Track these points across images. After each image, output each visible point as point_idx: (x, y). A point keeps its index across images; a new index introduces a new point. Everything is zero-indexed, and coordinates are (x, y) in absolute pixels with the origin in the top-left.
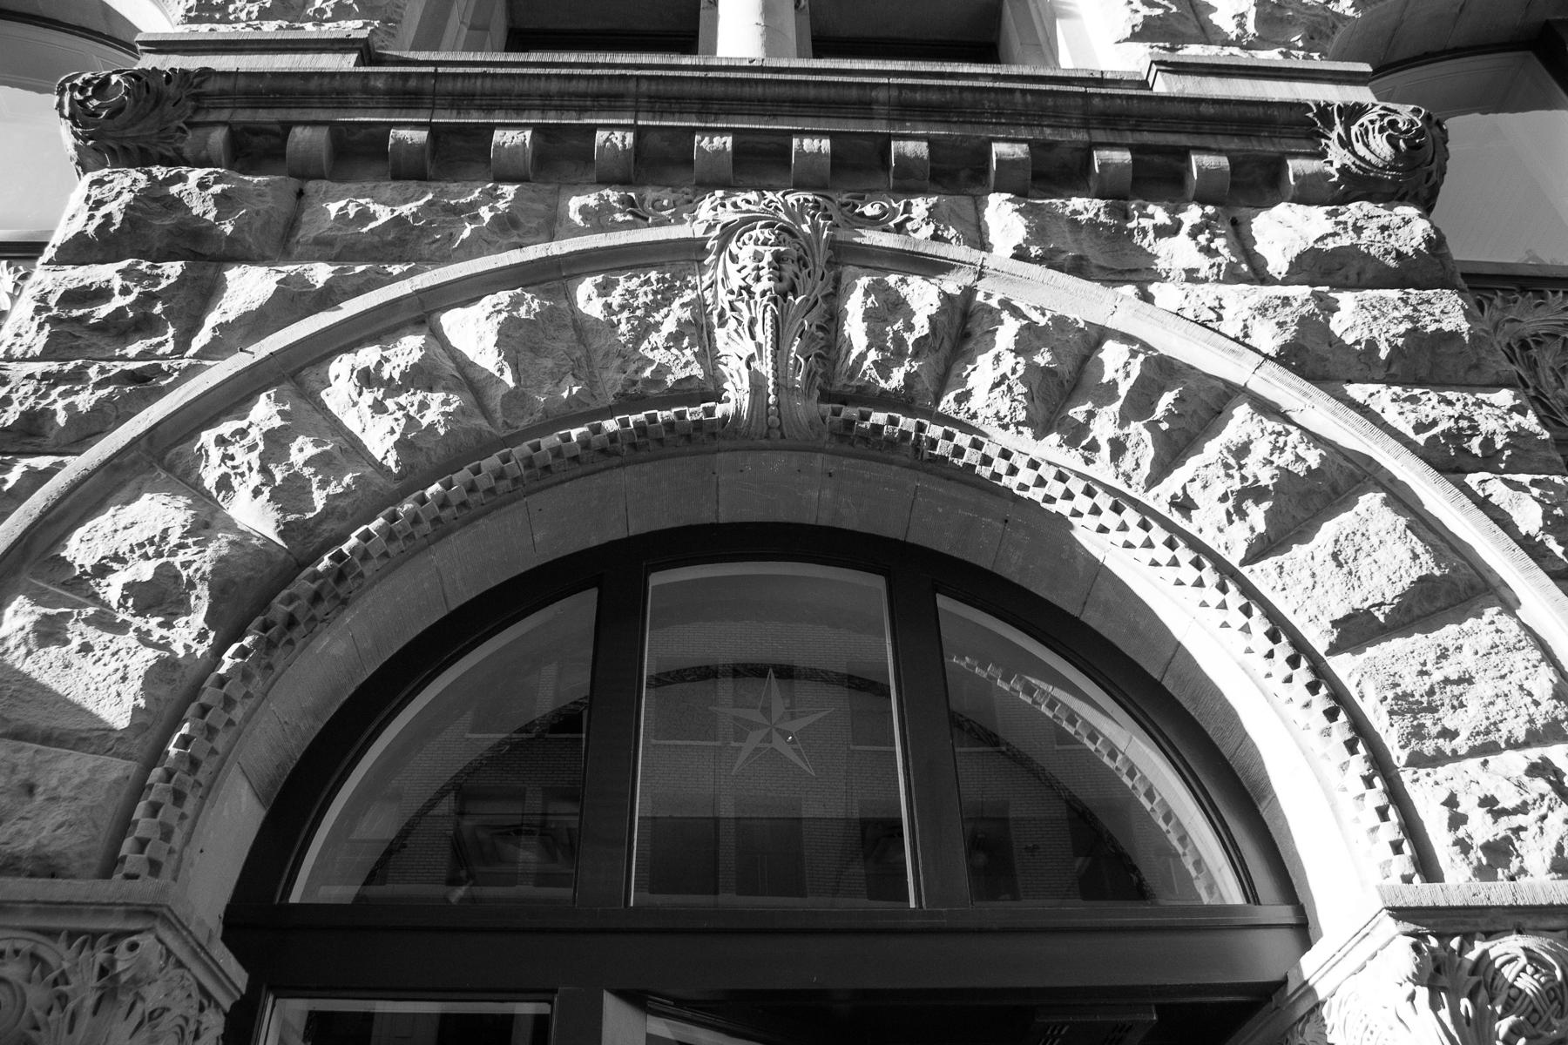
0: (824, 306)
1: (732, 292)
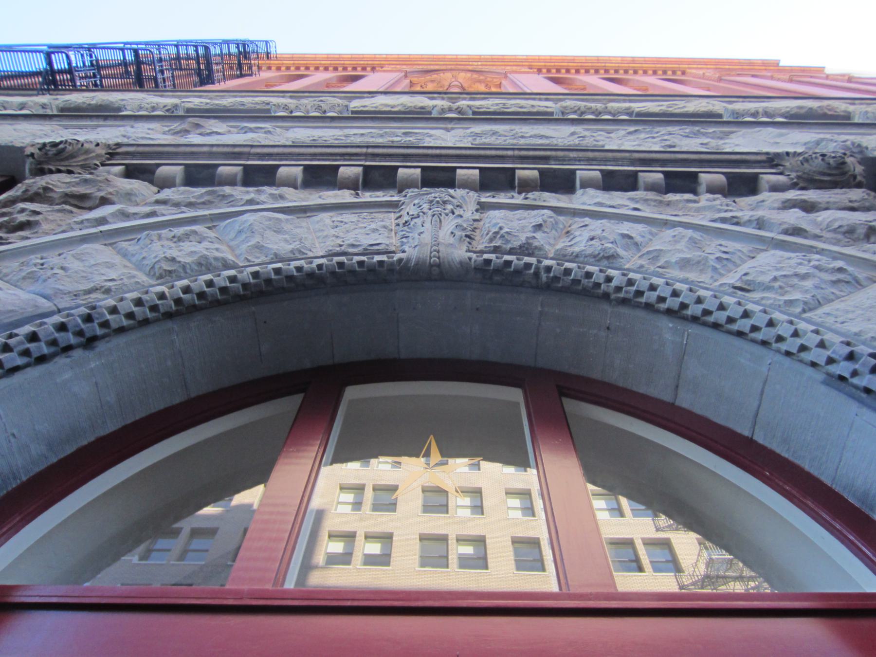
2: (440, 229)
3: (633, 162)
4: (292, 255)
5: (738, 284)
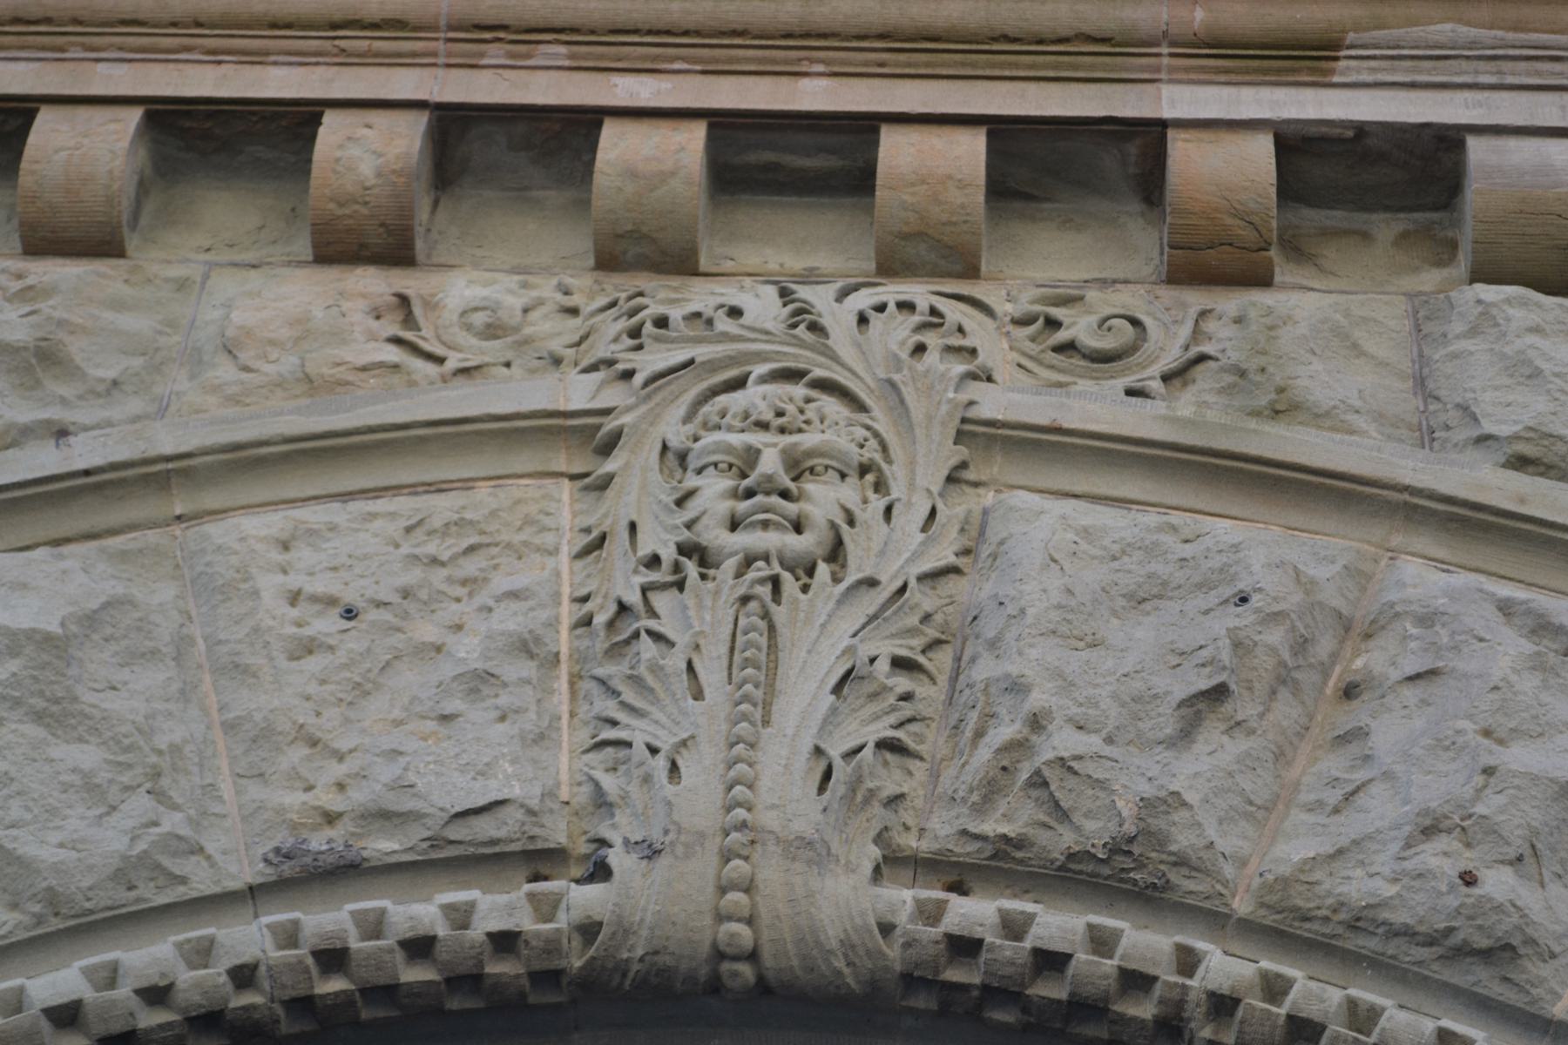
2: (766, 722)
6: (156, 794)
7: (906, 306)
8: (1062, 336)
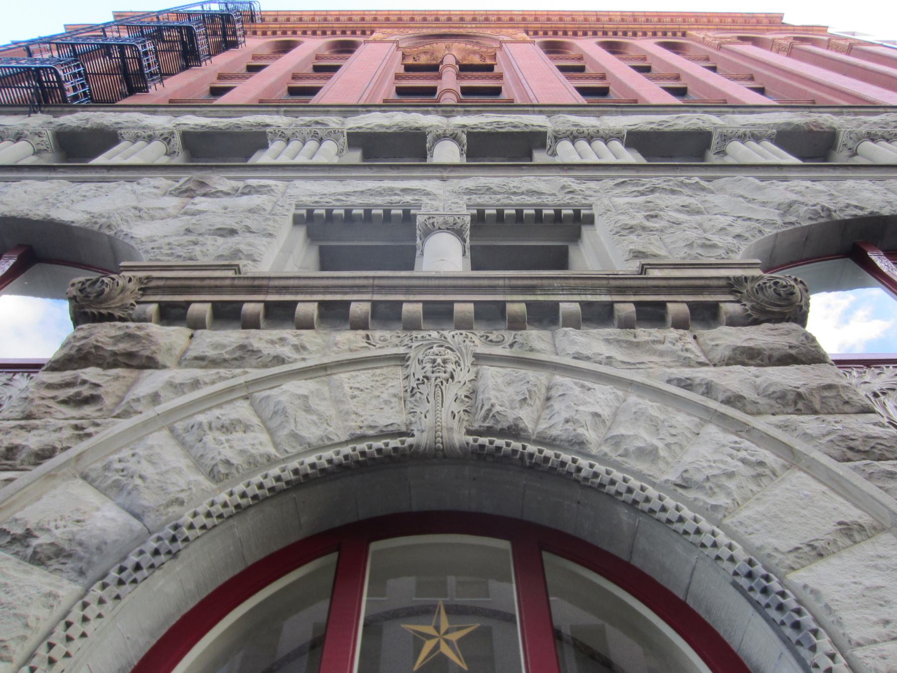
0: (470, 386)
1: (418, 380)
3: (611, 290)
4: (321, 443)
5: (679, 482)
6: (328, 424)
7: (461, 334)
8: (489, 339)
